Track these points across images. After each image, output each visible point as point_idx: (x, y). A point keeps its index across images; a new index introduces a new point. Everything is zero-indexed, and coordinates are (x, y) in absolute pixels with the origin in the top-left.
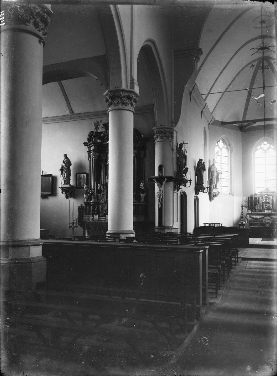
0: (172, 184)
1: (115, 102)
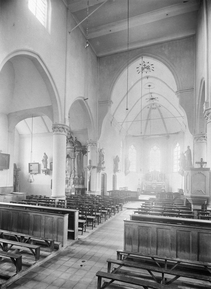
0: (96, 169)
1: (56, 130)
